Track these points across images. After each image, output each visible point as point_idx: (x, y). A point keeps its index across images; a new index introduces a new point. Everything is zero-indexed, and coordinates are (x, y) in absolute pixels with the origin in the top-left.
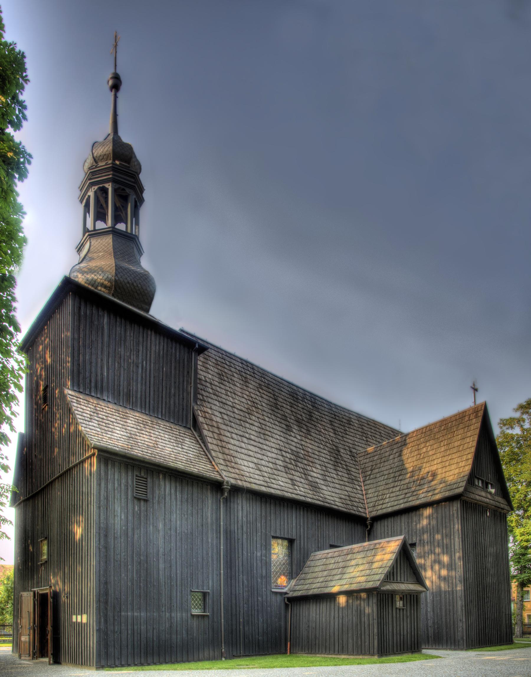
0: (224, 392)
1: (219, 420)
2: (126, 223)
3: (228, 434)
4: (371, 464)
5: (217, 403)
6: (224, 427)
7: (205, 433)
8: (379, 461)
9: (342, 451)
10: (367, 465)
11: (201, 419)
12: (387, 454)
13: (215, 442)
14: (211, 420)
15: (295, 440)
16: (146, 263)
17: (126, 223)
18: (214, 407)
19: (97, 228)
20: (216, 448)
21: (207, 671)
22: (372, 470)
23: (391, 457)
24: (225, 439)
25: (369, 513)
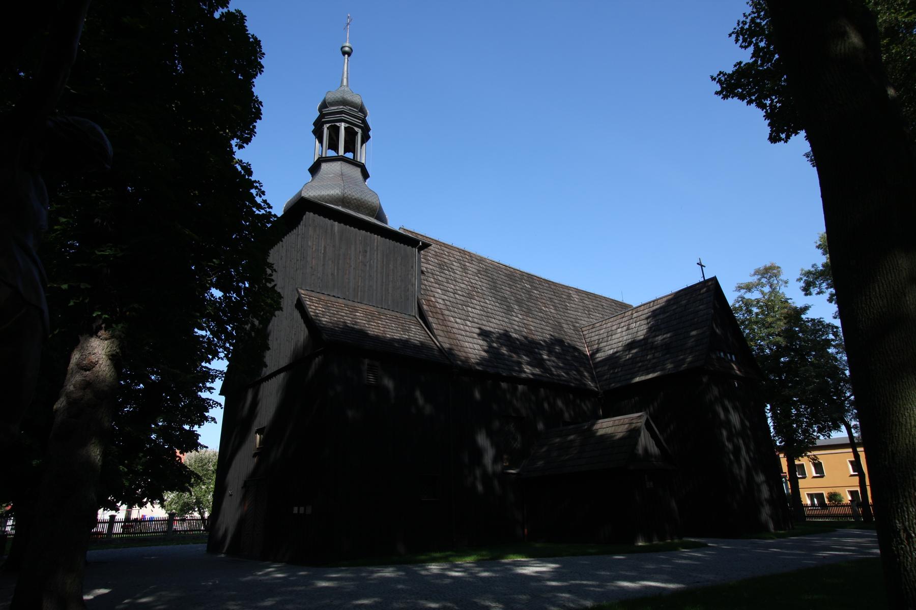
0: (444, 280)
1: (442, 307)
2: (354, 153)
3: (452, 319)
4: (597, 337)
5: (439, 291)
6: (446, 312)
7: (430, 319)
8: (605, 335)
9: (565, 326)
10: (593, 339)
11: (425, 307)
12: (615, 327)
13: (440, 327)
14: (435, 307)
15: (517, 319)
16: (634, 301)
17: (354, 153)
18: (437, 295)
19: (848, 441)
20: (441, 333)
21: (349, 97)
22: (599, 344)
23: (619, 330)
24: (449, 324)
25: (359, 170)
